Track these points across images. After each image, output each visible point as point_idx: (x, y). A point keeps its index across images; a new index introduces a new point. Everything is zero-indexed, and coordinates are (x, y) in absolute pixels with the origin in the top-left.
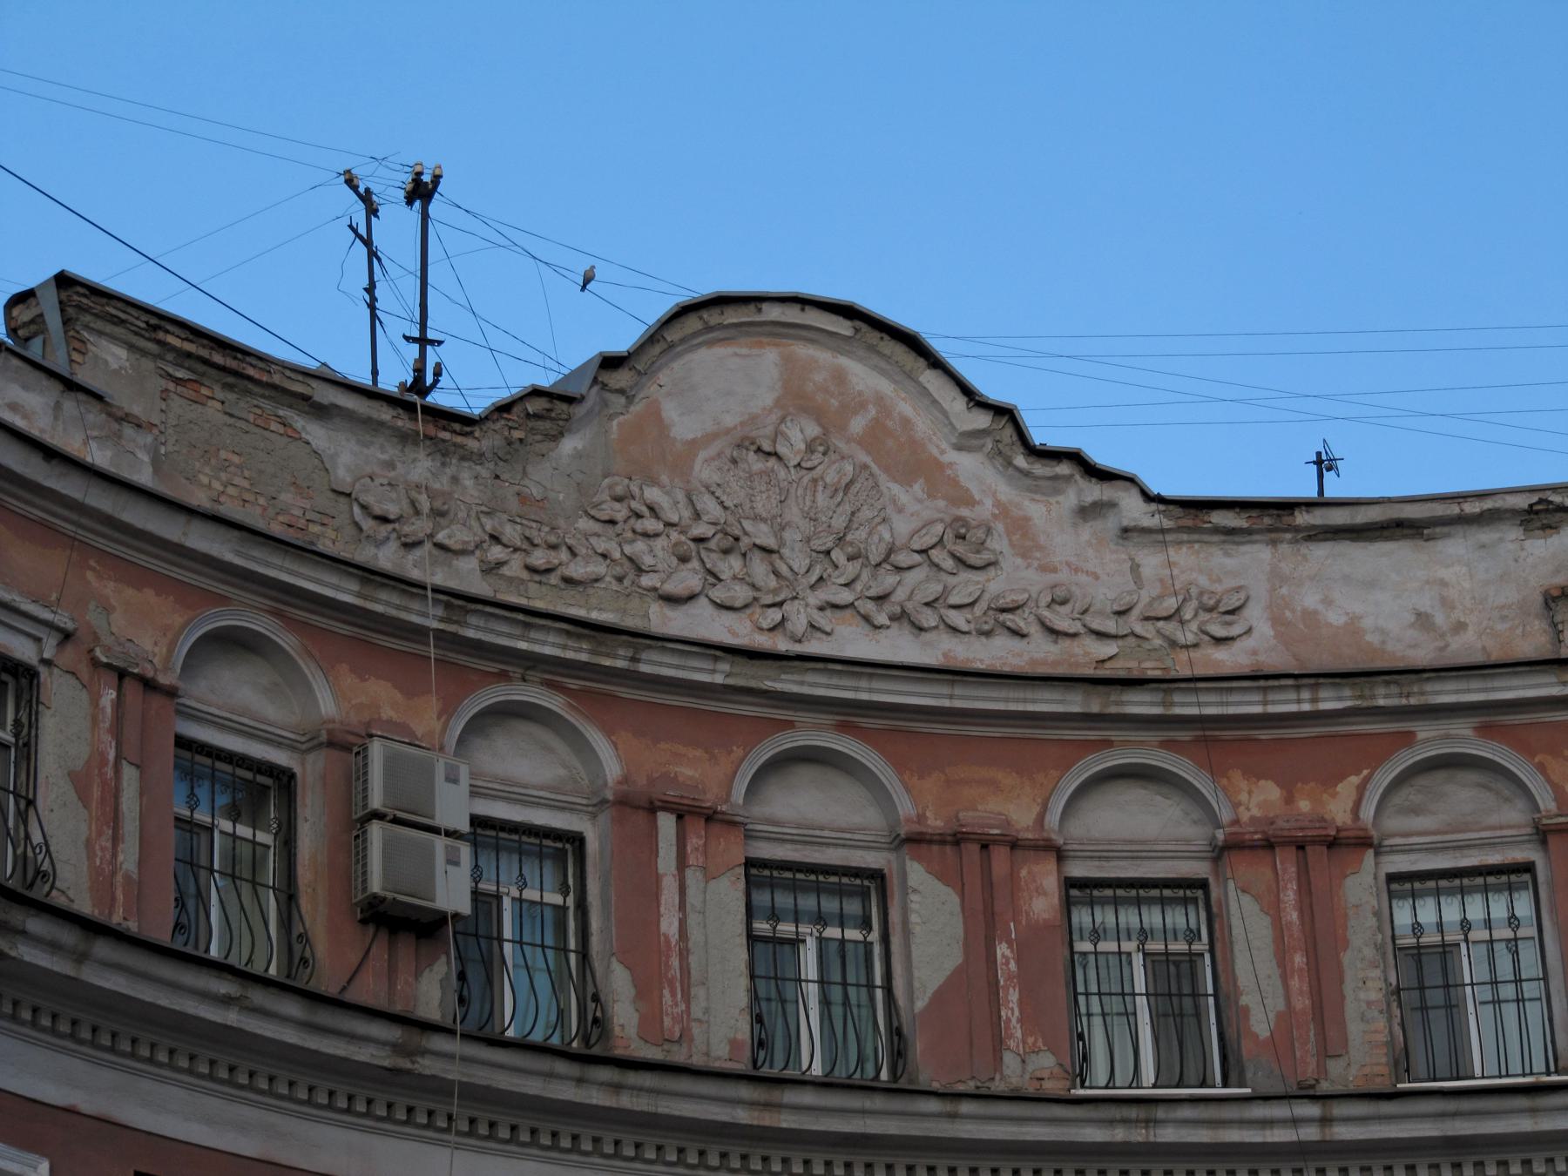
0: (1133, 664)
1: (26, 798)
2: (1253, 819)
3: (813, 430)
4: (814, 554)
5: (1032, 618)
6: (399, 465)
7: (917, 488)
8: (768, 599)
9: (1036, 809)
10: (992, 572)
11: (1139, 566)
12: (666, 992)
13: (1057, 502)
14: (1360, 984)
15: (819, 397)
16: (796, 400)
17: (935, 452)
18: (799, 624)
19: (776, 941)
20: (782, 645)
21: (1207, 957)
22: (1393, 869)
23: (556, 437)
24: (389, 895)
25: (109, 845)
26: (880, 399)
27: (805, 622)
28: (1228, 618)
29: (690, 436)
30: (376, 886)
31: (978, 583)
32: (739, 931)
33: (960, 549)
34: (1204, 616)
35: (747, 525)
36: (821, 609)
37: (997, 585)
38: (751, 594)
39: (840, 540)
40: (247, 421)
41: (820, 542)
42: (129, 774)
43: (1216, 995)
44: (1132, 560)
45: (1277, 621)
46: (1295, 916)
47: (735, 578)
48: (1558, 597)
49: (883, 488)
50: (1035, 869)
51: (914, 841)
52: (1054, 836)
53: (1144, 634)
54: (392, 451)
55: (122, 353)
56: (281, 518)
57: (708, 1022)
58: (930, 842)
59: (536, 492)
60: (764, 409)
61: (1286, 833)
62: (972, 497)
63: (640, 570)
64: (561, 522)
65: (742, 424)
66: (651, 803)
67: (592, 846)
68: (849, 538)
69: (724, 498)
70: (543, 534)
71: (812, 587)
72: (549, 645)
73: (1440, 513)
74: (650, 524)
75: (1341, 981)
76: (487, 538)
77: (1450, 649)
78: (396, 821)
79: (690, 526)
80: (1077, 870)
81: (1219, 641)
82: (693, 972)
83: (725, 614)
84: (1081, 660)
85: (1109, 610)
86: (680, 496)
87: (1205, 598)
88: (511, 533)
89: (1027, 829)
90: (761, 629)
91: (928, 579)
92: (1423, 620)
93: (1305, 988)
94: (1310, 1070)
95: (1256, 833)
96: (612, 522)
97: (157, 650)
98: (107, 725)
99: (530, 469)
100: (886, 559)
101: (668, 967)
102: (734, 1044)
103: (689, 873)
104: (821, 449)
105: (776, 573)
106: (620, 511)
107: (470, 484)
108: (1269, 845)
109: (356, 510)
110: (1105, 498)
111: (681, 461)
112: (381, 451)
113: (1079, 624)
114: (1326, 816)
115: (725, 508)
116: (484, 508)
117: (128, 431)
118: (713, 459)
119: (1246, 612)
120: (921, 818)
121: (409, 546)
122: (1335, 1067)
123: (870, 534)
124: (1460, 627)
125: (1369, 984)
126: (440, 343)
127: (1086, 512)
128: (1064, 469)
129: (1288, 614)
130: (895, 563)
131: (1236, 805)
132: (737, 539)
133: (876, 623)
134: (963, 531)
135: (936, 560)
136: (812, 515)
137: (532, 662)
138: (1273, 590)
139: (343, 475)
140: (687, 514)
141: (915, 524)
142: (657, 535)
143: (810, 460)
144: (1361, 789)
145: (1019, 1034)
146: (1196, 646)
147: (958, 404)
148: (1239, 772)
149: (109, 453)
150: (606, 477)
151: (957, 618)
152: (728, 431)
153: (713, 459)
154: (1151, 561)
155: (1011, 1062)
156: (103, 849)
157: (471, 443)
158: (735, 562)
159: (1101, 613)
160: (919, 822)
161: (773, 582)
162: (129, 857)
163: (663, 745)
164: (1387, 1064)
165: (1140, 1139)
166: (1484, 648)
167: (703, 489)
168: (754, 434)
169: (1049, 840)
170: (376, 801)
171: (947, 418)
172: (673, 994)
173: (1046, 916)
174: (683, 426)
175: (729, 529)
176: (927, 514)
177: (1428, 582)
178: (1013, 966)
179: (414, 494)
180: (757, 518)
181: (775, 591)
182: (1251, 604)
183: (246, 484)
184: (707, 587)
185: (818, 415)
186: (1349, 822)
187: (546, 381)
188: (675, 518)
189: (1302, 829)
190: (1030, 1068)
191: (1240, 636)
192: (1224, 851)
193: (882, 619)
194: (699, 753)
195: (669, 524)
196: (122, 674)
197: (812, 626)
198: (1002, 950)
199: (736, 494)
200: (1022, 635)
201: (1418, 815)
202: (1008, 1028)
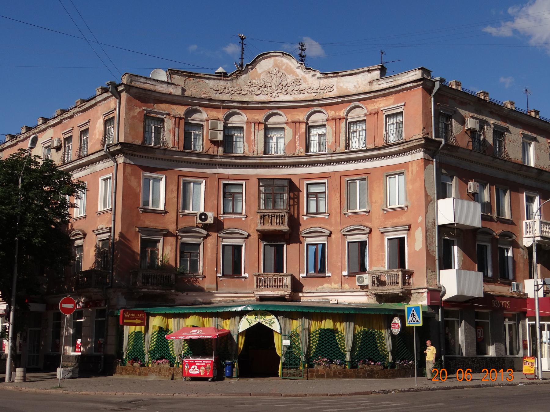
3: (277, 69)
16: (276, 65)
20: (273, 100)
26: (287, 63)
35: (267, 84)
37: (301, 87)
39: (280, 84)
45: (337, 88)
54: (218, 81)
59: (238, 83)
78: (212, 130)
92: (355, 86)
100: (286, 86)
101: (252, 143)
102: (261, 151)
107: (229, 84)
138: (337, 84)
151: (295, 92)
157: (229, 79)
158: (266, 89)
170: (209, 128)
176: (292, 79)
194: (258, 115)
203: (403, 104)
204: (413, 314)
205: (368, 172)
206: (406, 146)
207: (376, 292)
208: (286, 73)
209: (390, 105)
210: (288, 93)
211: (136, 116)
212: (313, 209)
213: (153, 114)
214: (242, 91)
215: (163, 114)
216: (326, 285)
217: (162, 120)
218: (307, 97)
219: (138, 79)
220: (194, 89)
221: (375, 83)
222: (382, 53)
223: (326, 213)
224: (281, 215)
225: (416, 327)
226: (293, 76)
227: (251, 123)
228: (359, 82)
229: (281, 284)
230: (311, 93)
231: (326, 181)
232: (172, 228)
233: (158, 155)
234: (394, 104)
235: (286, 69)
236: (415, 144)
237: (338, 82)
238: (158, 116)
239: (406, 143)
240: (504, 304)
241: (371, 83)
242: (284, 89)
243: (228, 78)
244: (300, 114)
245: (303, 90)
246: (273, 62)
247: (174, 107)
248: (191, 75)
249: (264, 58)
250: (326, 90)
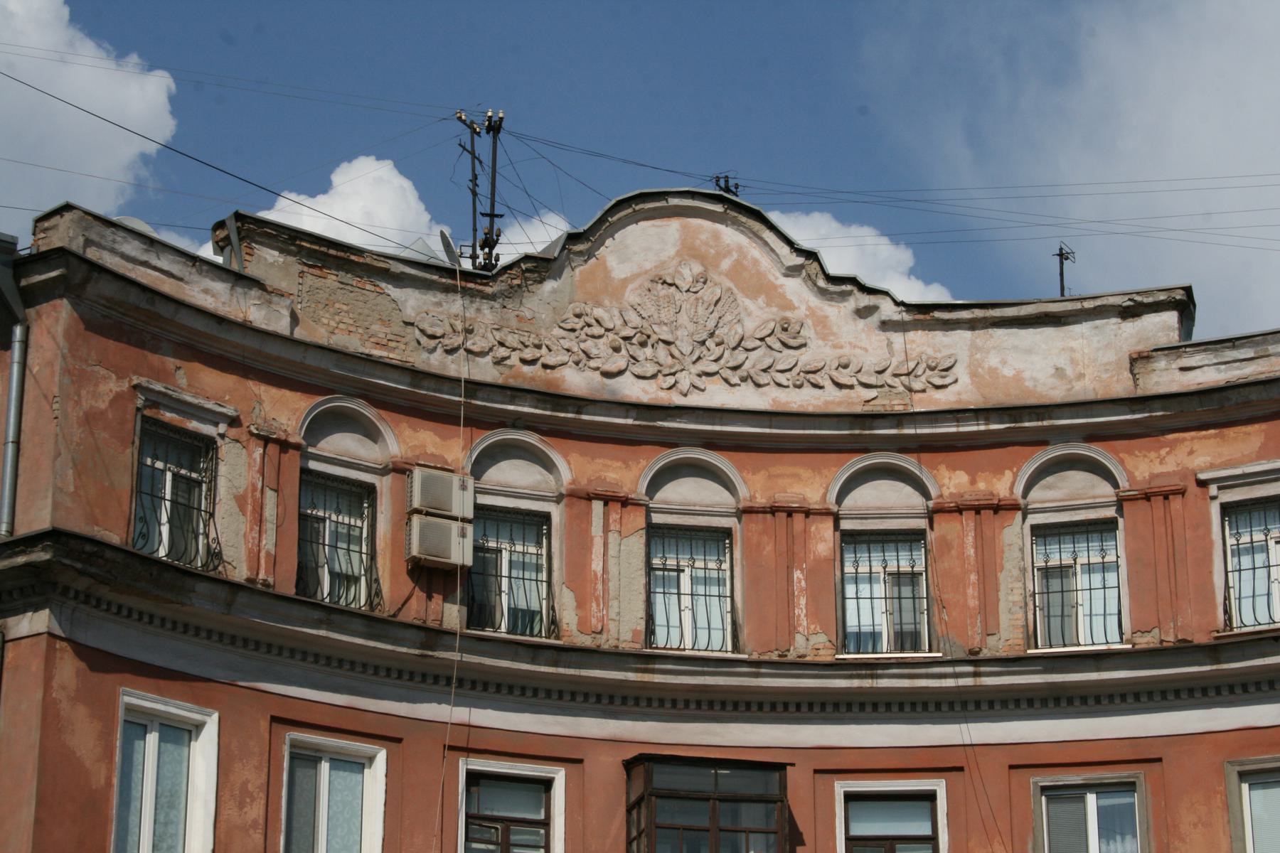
0: (886, 402)
1: (209, 512)
2: (951, 494)
3: (697, 268)
4: (695, 343)
5: (826, 376)
6: (444, 304)
7: (761, 300)
8: (666, 371)
9: (822, 491)
10: (803, 349)
11: (892, 343)
12: (594, 605)
13: (845, 307)
14: (1010, 592)
15: (703, 249)
16: (689, 251)
17: (772, 278)
18: (685, 383)
20: (678, 400)
21: (924, 574)
22: (1035, 522)
23: (541, 281)
24: (423, 557)
25: (257, 535)
26: (740, 249)
27: (689, 384)
28: (944, 373)
29: (623, 276)
30: (415, 552)
31: (794, 356)
32: (641, 567)
33: (784, 337)
34: (929, 372)
35: (656, 328)
36: (699, 376)
37: (806, 358)
38: (656, 368)
39: (712, 335)
40: (352, 285)
41: (699, 336)
42: (270, 497)
43: (927, 598)
44: (888, 339)
45: (973, 375)
46: (972, 552)
47: (646, 359)
48: (1136, 359)
49: (739, 301)
50: (821, 526)
51: (744, 512)
52: (831, 507)
53: (893, 384)
54: (440, 297)
56: (372, 340)
57: (619, 620)
58: (757, 512)
59: (528, 314)
60: (669, 257)
61: (968, 503)
62: (793, 305)
63: (589, 357)
64: (543, 331)
65: (656, 267)
66: (588, 495)
67: (556, 519)
68: (717, 332)
69: (642, 312)
70: (531, 339)
71: (694, 363)
73: (1070, 309)
74: (597, 330)
75: (998, 591)
76: (496, 343)
77: (1074, 390)
78: (428, 514)
79: (621, 330)
82: (610, 592)
83: (641, 381)
84: (856, 400)
85: (872, 370)
86: (616, 312)
87: (930, 362)
88: (512, 340)
89: (816, 503)
90: (662, 389)
91: (765, 355)
92: (1059, 372)
93: (976, 594)
94: (976, 643)
95: (952, 502)
96: (573, 330)
97: (290, 423)
98: (257, 468)
99: (524, 301)
100: (739, 345)
101: (595, 590)
102: (635, 632)
103: (610, 534)
104: (702, 280)
105: (673, 356)
106: (580, 323)
107: (486, 314)
108: (959, 510)
109: (417, 332)
110: (871, 304)
111: (617, 290)
112: (431, 298)
113: (854, 379)
114: (994, 492)
115: (643, 318)
116: (496, 326)
117: (275, 299)
118: (636, 289)
119: (954, 370)
120: (752, 498)
121: (451, 351)
122: (991, 641)
123: (730, 330)
124: (1081, 376)
125: (1015, 591)
126: (502, 216)
127: (863, 313)
128: (849, 287)
129: (980, 370)
130: (746, 347)
131: (941, 486)
132: (649, 337)
133: (732, 382)
134: (786, 326)
135: (769, 344)
136: (695, 320)
138: (971, 356)
139: (410, 313)
140: (619, 322)
141: (757, 324)
142: (600, 337)
143: (695, 287)
144: (1015, 476)
145: (805, 623)
146: (924, 391)
147: (783, 250)
148: (944, 466)
149: (263, 312)
150: (570, 303)
151: (781, 378)
152: (646, 272)
153: (636, 289)
154: (897, 338)
155: (799, 639)
156: (253, 538)
157: (488, 290)
158: (648, 351)
159: (868, 373)
160: (751, 501)
161: (670, 360)
162: (268, 542)
163: (598, 461)
164: (1023, 638)
165: (868, 686)
166: (1094, 389)
167: (630, 308)
168: (662, 273)
169: (829, 509)
170: (416, 504)
171: (779, 258)
172: (598, 605)
173: (825, 554)
175: (644, 331)
176: (765, 316)
177: (1063, 349)
178: (803, 583)
179: (453, 321)
180: (662, 323)
181: (671, 367)
182: (957, 365)
183: (351, 322)
184: (630, 365)
185: (701, 258)
186: (1008, 495)
187: (531, 250)
188: (611, 326)
189: (978, 500)
190: (811, 643)
191: (950, 384)
193: (735, 380)
194: (619, 464)
195: (608, 330)
197: (694, 386)
198: (797, 574)
199: (650, 309)
200: (821, 387)
201: (1051, 489)
202: (798, 620)
208: (735, 290)
209: (1241, 462)
210: (744, 379)
211: (103, 413)
213: (172, 410)
214: (544, 350)
215: (214, 418)
217: (207, 447)
218: (832, 403)
219: (114, 241)
220: (337, 318)
222: (1062, 256)
226: (768, 305)
227: (589, 498)
228: (1078, 356)
230: (851, 387)
231: (939, 786)
233: (202, 605)
234: (1261, 455)
237: (978, 349)
238: (194, 425)
241: (1139, 360)
243: (486, 284)
244: (805, 473)
245: (814, 372)
246: (677, 235)
247: (267, 393)
248: (332, 252)
249: (623, 224)
250: (923, 379)
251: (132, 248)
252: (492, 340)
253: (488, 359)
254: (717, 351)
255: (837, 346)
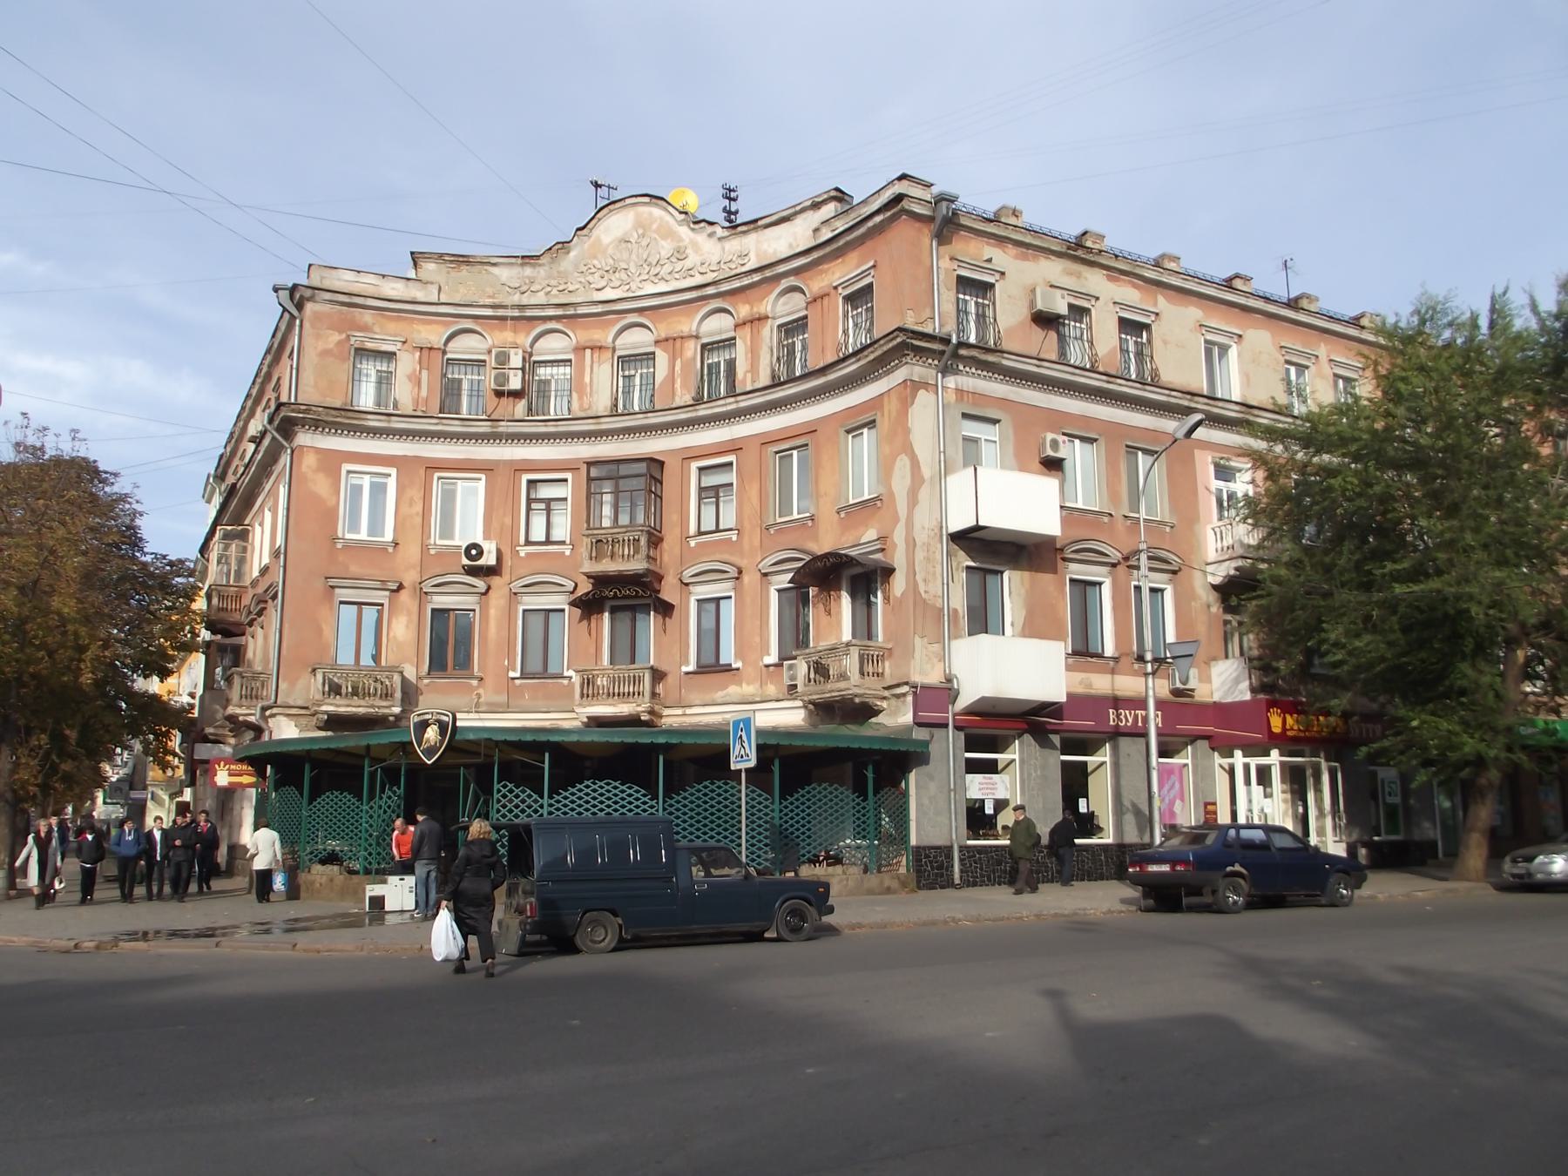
3: (640, 231)
7: (669, 241)
19: (629, 376)
23: (568, 253)
37: (688, 263)
55: (433, 265)
72: (551, 312)
74: (593, 270)
80: (705, 340)
81: (743, 265)
88: (553, 282)
102: (606, 408)
127: (711, 235)
128: (703, 224)
137: (550, 318)
151: (677, 276)
155: (677, 399)
174: (606, 239)
192: (736, 326)
196: (422, 348)
203: (871, 264)
204: (741, 736)
205: (810, 430)
206: (872, 357)
207: (810, 697)
212: (709, 524)
216: (733, 690)
221: (824, 230)
223: (568, 542)
224: (631, 538)
225: (747, 770)
229: (636, 689)
232: (410, 577)
235: (657, 231)
236: (885, 348)
239: (870, 350)
240: (1367, 730)
241: (816, 230)
242: (654, 271)
251: (350, 276)
252: (544, 284)
253: (542, 293)
254: (647, 269)
255: (702, 255)
